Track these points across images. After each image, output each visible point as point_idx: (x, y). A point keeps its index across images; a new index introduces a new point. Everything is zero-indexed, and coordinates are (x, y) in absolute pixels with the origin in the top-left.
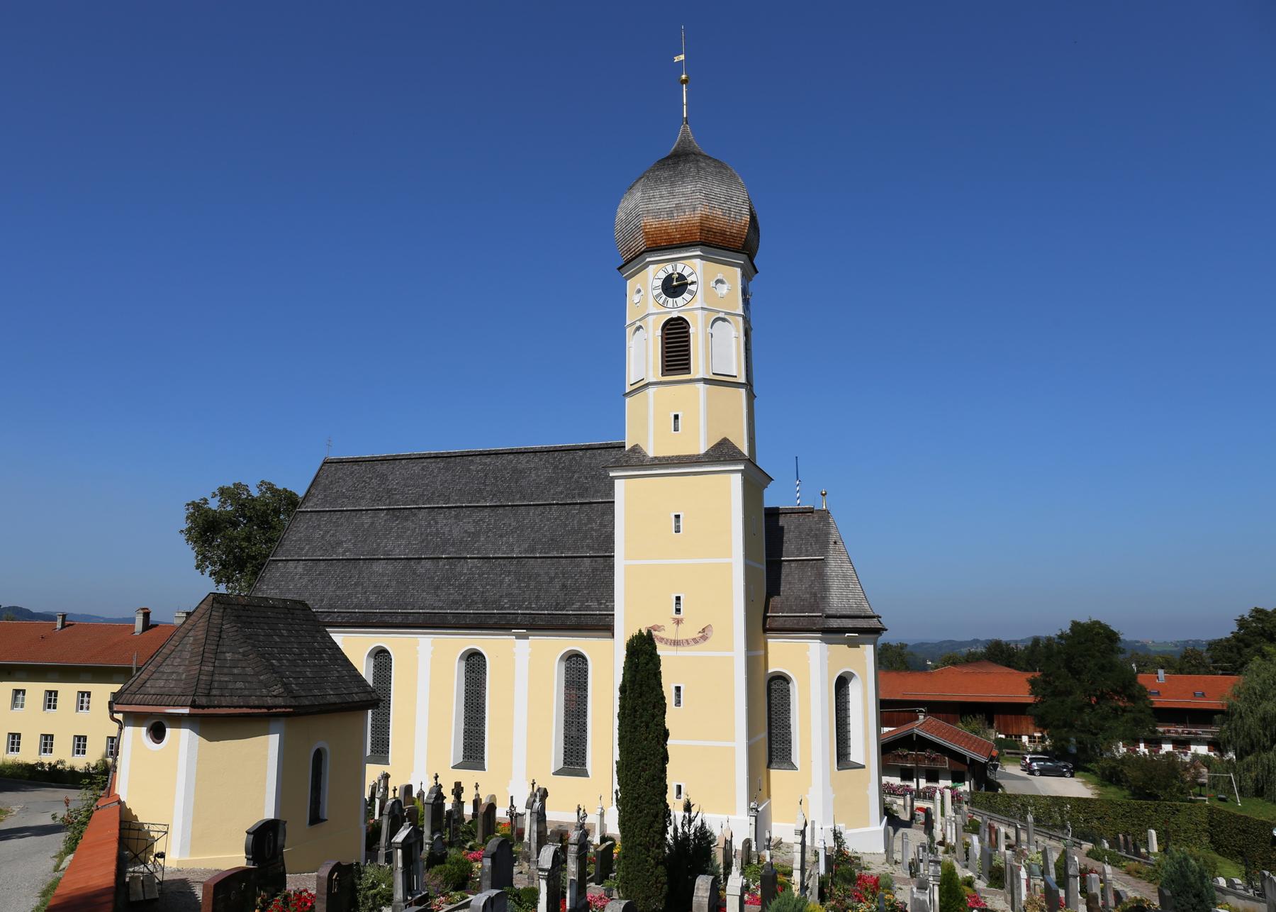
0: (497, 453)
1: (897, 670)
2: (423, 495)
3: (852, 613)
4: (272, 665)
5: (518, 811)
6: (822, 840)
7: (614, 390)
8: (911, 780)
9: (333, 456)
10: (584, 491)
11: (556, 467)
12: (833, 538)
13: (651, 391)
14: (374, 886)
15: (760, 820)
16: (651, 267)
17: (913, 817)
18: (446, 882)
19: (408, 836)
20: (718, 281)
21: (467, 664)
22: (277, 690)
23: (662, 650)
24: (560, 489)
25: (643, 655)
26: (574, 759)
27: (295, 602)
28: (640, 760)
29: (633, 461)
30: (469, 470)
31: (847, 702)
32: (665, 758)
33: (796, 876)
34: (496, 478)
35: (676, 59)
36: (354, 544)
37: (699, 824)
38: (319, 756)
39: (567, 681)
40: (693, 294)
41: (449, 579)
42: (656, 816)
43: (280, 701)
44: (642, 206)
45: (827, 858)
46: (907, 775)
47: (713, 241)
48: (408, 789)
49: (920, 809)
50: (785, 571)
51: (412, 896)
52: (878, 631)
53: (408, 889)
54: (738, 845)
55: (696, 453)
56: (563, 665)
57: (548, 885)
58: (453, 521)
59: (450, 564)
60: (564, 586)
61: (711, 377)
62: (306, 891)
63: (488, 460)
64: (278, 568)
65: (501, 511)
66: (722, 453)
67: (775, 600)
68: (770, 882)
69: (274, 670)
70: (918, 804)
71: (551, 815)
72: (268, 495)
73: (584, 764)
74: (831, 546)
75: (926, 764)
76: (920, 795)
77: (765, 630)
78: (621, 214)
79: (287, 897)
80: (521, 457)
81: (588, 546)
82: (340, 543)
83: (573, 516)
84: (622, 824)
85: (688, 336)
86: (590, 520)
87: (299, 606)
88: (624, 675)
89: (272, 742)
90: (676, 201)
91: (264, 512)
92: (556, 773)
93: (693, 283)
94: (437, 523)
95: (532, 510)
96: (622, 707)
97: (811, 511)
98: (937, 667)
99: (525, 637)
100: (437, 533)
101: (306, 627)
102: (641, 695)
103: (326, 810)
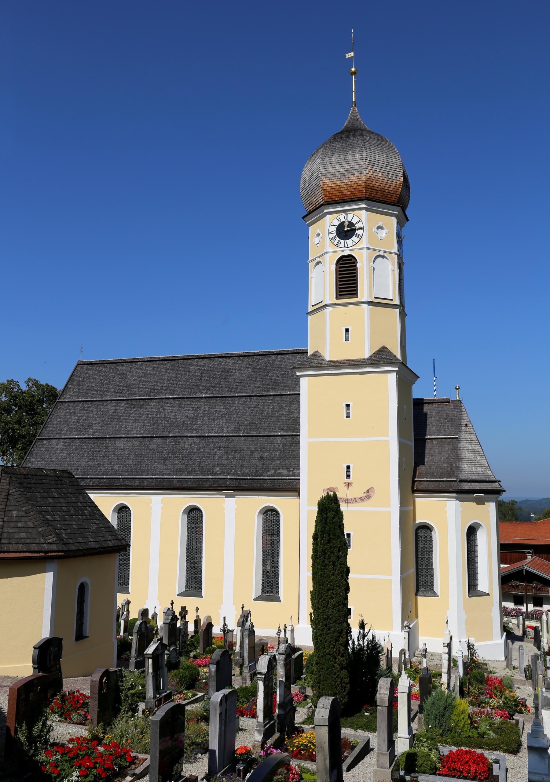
0: (210, 357)
1: (510, 521)
2: (154, 389)
3: (479, 479)
4: (47, 520)
5: (229, 628)
6: (460, 652)
7: (299, 310)
8: (522, 604)
10: (276, 386)
11: (255, 368)
12: (464, 422)
13: (328, 310)
14: (133, 687)
15: (411, 634)
16: (328, 217)
17: (524, 633)
18: (180, 683)
19: (157, 649)
20: (379, 228)
21: (188, 517)
22: (52, 538)
23: (343, 507)
24: (258, 384)
25: (329, 512)
26: (270, 588)
27: (63, 471)
28: (328, 590)
29: (314, 364)
30: (188, 370)
31: (475, 546)
32: (347, 589)
33: (445, 678)
34: (209, 376)
35: (347, 56)
36: (102, 426)
37: (371, 638)
38: (82, 588)
39: (264, 530)
41: (174, 453)
42: (341, 632)
43: (54, 547)
44: (321, 170)
45: (464, 664)
46: (518, 601)
47: (375, 197)
48: (145, 613)
49: (530, 627)
50: (428, 446)
51: (160, 694)
52: (498, 492)
53: (157, 689)
54: (396, 654)
57: (264, 685)
59: (175, 442)
60: (262, 458)
61: (373, 300)
62: (78, 691)
63: (203, 362)
64: (43, 445)
65: (213, 401)
66: (381, 358)
67: (421, 469)
68: (426, 681)
69: (48, 523)
70: (528, 623)
71: (259, 632)
72: (34, 388)
73: (277, 592)
74: (463, 428)
75: (533, 593)
76: (528, 616)
77: (414, 491)
78: (305, 176)
79: (64, 696)
80: (229, 361)
81: (279, 428)
82: (90, 426)
83: (268, 405)
84: (315, 638)
85: (356, 269)
87: (65, 475)
88: (316, 526)
91: (31, 402)
92: (256, 599)
93: (359, 229)
94: (164, 410)
95: (237, 400)
96: (315, 550)
97: (448, 401)
98: (539, 519)
99: (233, 496)
100: (165, 418)
101: (70, 489)
102: (329, 541)
103: (88, 630)
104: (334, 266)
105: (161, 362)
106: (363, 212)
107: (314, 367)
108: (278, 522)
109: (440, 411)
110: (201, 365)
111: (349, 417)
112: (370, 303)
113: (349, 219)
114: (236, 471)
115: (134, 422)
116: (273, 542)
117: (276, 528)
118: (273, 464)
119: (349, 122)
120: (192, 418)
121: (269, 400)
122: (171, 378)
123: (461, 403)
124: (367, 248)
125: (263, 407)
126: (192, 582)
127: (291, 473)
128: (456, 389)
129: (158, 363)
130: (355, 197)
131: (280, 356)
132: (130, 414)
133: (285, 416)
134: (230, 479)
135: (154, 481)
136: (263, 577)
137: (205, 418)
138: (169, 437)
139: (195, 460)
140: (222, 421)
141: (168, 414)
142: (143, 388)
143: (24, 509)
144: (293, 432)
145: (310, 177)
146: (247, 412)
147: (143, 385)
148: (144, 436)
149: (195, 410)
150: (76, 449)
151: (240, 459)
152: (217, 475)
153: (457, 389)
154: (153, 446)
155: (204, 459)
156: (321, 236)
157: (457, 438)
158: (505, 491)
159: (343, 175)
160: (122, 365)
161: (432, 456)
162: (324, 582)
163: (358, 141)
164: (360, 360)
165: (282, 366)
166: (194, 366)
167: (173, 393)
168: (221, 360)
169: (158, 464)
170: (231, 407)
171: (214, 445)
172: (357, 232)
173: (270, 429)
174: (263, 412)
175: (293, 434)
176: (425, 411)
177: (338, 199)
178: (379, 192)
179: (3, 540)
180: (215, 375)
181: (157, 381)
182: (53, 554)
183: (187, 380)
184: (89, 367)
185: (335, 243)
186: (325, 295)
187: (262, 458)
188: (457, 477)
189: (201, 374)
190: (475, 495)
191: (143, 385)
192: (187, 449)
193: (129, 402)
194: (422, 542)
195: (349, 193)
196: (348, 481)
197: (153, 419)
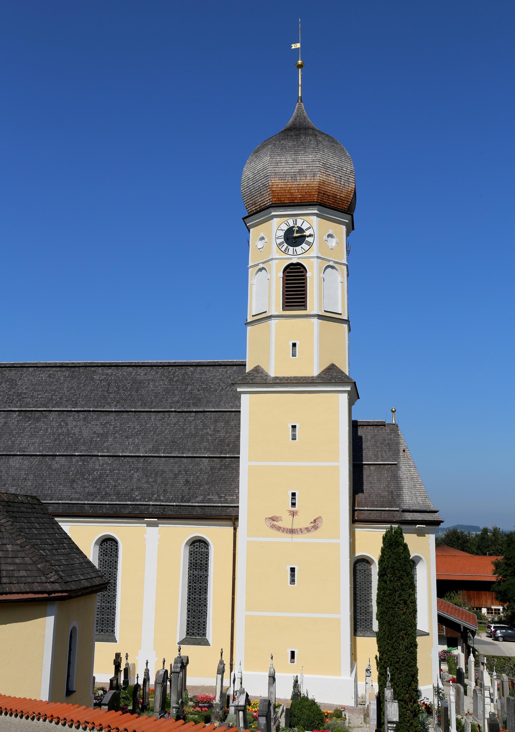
0: (117, 366)
2: (52, 399)
7: (238, 319)
13: (274, 322)
16: (275, 220)
20: (330, 236)
24: (176, 399)
29: (258, 380)
30: (92, 379)
34: (118, 387)
35: (294, 46)
39: (190, 563)
40: (310, 244)
41: (83, 475)
43: (57, 587)
44: (271, 169)
52: (437, 523)
55: (310, 375)
58: (81, 423)
59: (83, 461)
60: (187, 482)
63: (109, 371)
65: (125, 415)
66: (331, 376)
67: (360, 497)
73: (204, 635)
74: (401, 453)
80: (139, 370)
85: (305, 279)
86: (205, 426)
89: (49, 621)
90: (297, 168)
93: (310, 236)
94: (67, 424)
95: (153, 416)
97: (383, 425)
99: (156, 525)
100: (68, 434)
104: (281, 274)
105: (59, 369)
106: (314, 218)
107: (258, 383)
108: (207, 555)
109: (375, 435)
110: (107, 374)
111: (295, 439)
112: (320, 317)
113: (299, 224)
114: (159, 496)
115: (30, 437)
116: (201, 577)
117: (204, 562)
118: (201, 489)
119: (296, 119)
120: (102, 434)
121: (191, 417)
122: (72, 388)
123: (398, 427)
124: (318, 257)
125: (185, 425)
126: (103, 624)
127: (223, 499)
129: (54, 369)
130: (305, 201)
131: (199, 368)
132: (25, 428)
133: (211, 435)
134: (153, 505)
135: (61, 507)
136: (188, 617)
137: (117, 435)
138: (75, 455)
139: (109, 482)
140: (138, 438)
141: (72, 429)
142: (38, 398)
143: (18, 542)
144: (221, 453)
145: (255, 175)
146: (166, 429)
147: (38, 395)
148: (44, 454)
149: (104, 425)
151: (162, 482)
152: (137, 501)
154: (55, 466)
155: (119, 481)
156: (266, 240)
157: (396, 464)
158: (443, 522)
159: (294, 177)
160: (10, 370)
161: (371, 483)
162: (396, 622)
163: (311, 140)
164: (309, 378)
165: (203, 380)
166: (99, 375)
167: (76, 405)
168: (130, 369)
169: (64, 486)
170: (146, 424)
171: (130, 466)
172: (307, 239)
173: (194, 450)
174: (184, 430)
175: (222, 456)
176: (359, 434)
178: (331, 197)
179: (3, 579)
180: (125, 386)
181: (55, 391)
182: (57, 595)
183: (91, 391)
185: (283, 249)
186: (269, 305)
187: (187, 482)
188: (399, 506)
190: (418, 526)
191: (38, 395)
192: (97, 470)
193: (23, 413)
194: (360, 577)
195: (300, 196)
196: (293, 509)
197: (54, 434)
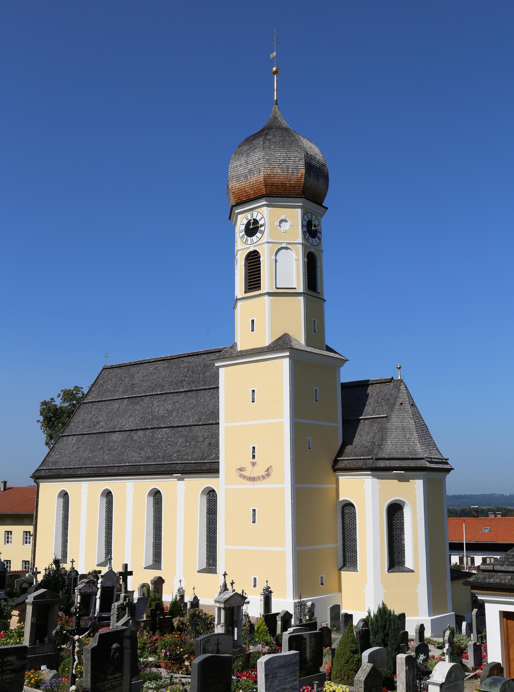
0: (198, 354)
9: (109, 364)
16: (240, 217)
36: (106, 423)
40: (262, 233)
47: (275, 192)
56: (205, 498)
59: (152, 432)
65: (190, 394)
66: (282, 344)
74: (397, 407)
77: (335, 470)
82: (98, 423)
99: (183, 479)
106: (265, 209)
112: (270, 294)
113: (254, 217)
124: (268, 242)
128: (398, 368)
129: (159, 362)
150: (84, 444)
153: (399, 368)
158: (453, 469)
177: (245, 199)
178: (280, 187)
184: (110, 370)
185: (244, 241)
189: (188, 370)
193: (130, 400)
195: (252, 192)
196: (253, 460)
